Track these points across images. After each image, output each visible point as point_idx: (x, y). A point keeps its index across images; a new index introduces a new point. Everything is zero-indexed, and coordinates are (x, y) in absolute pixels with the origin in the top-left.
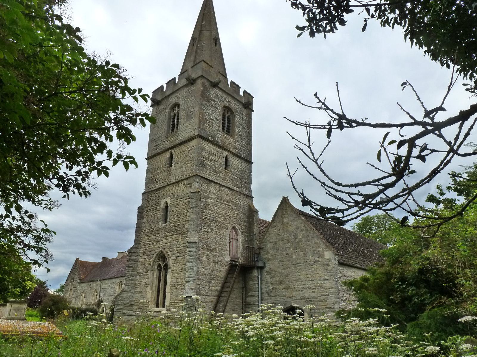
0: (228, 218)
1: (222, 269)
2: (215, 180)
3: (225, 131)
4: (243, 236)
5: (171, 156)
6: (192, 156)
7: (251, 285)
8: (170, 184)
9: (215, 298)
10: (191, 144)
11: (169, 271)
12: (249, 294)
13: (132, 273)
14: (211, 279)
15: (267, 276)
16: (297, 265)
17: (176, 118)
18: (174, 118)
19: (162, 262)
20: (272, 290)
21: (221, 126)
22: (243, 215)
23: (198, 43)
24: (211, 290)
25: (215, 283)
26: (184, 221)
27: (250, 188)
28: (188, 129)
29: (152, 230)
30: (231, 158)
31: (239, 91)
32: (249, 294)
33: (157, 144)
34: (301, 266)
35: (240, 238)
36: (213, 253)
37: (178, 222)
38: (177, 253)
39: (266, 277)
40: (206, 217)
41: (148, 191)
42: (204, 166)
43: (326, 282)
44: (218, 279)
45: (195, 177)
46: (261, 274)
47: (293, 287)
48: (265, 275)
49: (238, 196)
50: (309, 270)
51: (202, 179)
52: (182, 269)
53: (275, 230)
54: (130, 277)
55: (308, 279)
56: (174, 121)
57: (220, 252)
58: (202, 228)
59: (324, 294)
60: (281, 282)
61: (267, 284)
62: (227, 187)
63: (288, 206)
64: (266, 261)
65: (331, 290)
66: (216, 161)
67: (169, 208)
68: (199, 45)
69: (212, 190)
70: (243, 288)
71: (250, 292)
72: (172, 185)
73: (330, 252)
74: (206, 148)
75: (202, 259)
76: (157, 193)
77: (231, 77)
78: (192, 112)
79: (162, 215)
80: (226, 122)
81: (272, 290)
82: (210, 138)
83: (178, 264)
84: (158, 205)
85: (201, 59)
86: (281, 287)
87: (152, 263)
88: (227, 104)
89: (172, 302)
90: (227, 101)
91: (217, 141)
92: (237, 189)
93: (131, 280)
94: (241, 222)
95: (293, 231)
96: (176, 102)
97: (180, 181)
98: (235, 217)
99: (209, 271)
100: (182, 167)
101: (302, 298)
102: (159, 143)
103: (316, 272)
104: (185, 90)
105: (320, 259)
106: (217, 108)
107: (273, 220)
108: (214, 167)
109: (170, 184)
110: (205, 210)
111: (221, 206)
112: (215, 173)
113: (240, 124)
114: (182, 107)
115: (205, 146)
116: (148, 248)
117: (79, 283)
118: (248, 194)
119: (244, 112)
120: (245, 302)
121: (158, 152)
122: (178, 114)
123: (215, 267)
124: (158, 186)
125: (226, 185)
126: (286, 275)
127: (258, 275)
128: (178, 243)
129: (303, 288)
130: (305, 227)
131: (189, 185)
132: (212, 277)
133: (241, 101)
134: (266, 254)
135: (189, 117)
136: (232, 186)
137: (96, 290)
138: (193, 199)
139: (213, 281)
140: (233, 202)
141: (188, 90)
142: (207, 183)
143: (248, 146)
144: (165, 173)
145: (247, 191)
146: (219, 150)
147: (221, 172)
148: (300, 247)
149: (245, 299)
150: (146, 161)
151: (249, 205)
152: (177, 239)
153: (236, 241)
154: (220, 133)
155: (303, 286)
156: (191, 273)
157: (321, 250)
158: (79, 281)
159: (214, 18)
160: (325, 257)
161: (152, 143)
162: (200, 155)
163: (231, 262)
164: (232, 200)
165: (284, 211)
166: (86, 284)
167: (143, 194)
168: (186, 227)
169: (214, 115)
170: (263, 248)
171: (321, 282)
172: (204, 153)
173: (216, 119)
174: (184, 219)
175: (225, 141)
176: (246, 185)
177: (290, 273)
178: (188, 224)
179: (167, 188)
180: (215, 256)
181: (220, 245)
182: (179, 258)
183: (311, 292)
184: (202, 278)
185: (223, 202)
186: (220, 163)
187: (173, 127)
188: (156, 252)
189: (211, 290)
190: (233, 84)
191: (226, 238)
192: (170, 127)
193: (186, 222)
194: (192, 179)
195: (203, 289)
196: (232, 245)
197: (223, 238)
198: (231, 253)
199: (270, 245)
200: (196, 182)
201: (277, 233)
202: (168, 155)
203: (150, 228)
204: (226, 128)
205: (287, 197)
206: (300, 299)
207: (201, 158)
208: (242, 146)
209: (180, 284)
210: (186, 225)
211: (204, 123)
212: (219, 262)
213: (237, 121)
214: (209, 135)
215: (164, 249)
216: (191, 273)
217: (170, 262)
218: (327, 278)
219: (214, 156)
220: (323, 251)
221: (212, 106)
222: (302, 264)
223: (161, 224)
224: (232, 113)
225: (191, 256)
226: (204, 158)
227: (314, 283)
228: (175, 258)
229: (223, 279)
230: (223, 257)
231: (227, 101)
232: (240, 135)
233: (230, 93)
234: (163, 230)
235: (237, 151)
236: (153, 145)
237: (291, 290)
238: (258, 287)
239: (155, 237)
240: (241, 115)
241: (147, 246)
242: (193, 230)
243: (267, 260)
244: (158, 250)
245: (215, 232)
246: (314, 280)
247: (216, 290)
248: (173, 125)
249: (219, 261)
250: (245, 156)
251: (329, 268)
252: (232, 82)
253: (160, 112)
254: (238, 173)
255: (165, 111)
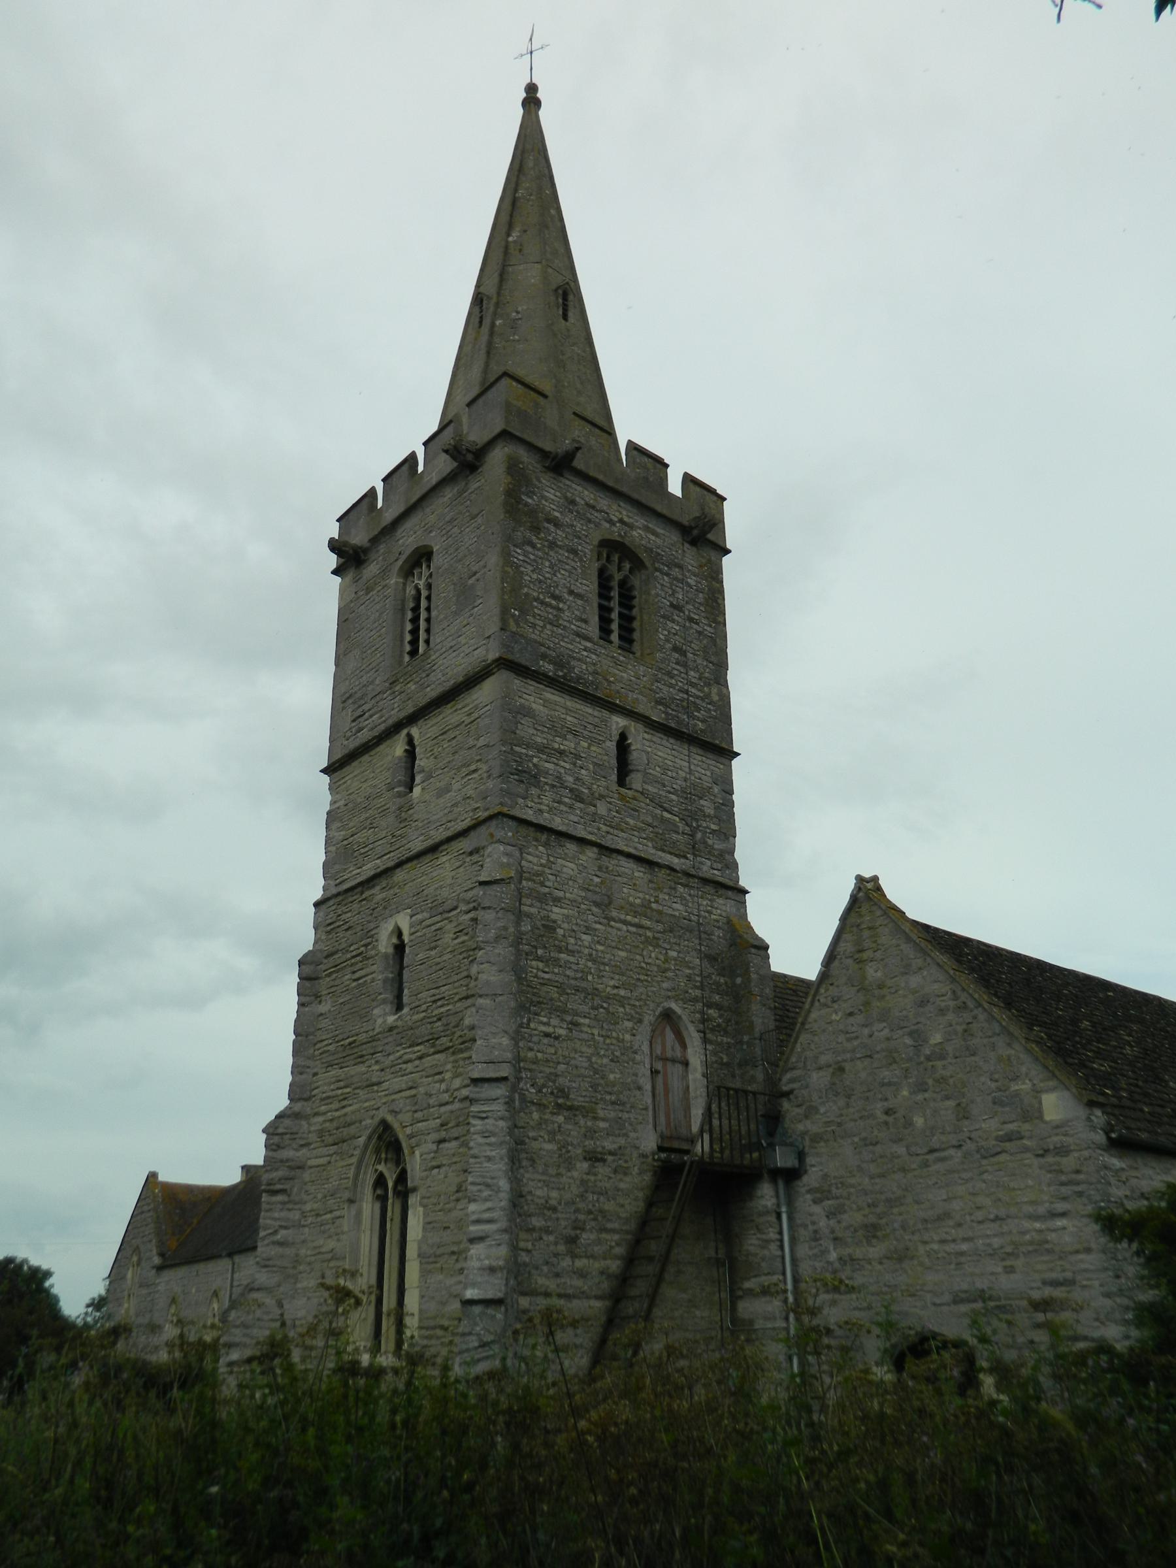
0: (642, 977)
1: (622, 1185)
2: (581, 832)
3: (615, 637)
4: (709, 1047)
5: (411, 754)
6: (482, 742)
7: (752, 1249)
8: (409, 860)
9: (598, 1304)
10: (474, 697)
11: (413, 1200)
12: (747, 1285)
13: (283, 1214)
14: (579, 1226)
15: (817, 1209)
16: (930, 1157)
17: (424, 604)
18: (416, 609)
19: (389, 1165)
20: (837, 1265)
21: (595, 620)
22: (706, 963)
23: (495, 315)
24: (582, 1274)
25: (599, 1242)
26: (461, 999)
27: (732, 852)
28: (464, 641)
29: (350, 1044)
30: (640, 739)
31: (664, 481)
32: (747, 1285)
33: (359, 712)
34: (951, 1158)
35: (696, 1056)
36: (582, 1122)
37: (439, 1003)
38: (442, 1125)
39: (811, 1210)
40: (547, 976)
41: (334, 891)
42: (527, 776)
43: (1059, 1223)
44: (609, 1226)
45: (494, 822)
46: (790, 1204)
47: (922, 1249)
48: (805, 1203)
49: (680, 889)
50: (985, 1176)
51: (523, 830)
52: (457, 1191)
53: (834, 1017)
54: (275, 1232)
55: (979, 1215)
56: (415, 620)
57: (613, 1115)
58: (529, 1020)
59: (1054, 1275)
60: (872, 1232)
61: (816, 1240)
62: (629, 856)
63: (879, 913)
64: (807, 1143)
65: (1082, 1261)
66: (578, 757)
67: (407, 950)
68: (498, 322)
69: (569, 868)
70: (719, 1263)
71: (748, 1279)
72: (415, 862)
73: (1066, 1094)
74: (534, 706)
75: (535, 1145)
76: (364, 896)
77: (626, 431)
78: (475, 573)
79: (385, 981)
80: (615, 604)
81: (837, 1265)
82: (548, 668)
83: (443, 1169)
84: (369, 944)
85: (501, 369)
86: (875, 1251)
87: (353, 1169)
88: (615, 533)
89: (427, 1328)
90: (611, 522)
91: (579, 678)
92: (675, 861)
93: (280, 1244)
94: (698, 993)
95: (904, 1013)
96: (421, 544)
97: (441, 843)
98: (670, 974)
99: (567, 1196)
100: (447, 789)
101: (963, 1295)
102: (366, 707)
103: (1012, 1185)
104: (449, 493)
105: (1027, 1126)
106: (574, 552)
107: (824, 976)
108: (571, 779)
109: (409, 860)
110: (540, 952)
111: (609, 929)
112: (579, 805)
113: (672, 605)
114: (437, 560)
115: (532, 699)
116: (337, 1114)
117: (160, 1268)
118: (721, 879)
119: (690, 557)
120: (734, 1321)
121: (364, 741)
122: (429, 587)
123: (592, 1178)
124: (368, 870)
125: (626, 849)
126: (888, 1200)
127: (778, 1205)
128: (443, 1086)
129: (962, 1254)
130: (955, 997)
131: (475, 858)
132: (581, 1217)
133: (675, 516)
134: (806, 1117)
135: (465, 596)
136: (653, 851)
137: (216, 1294)
138: (489, 908)
139: (586, 1237)
140: (660, 912)
141: (460, 493)
142: (546, 845)
143: (714, 690)
144: (391, 819)
145: (719, 866)
146: (590, 711)
147: (601, 797)
148: (941, 1081)
149: (734, 1309)
150: (326, 779)
151: (729, 922)
152: (436, 1070)
153: (679, 1068)
154: (589, 645)
155: (964, 1247)
156: (489, 1204)
157: (1024, 1086)
158: (157, 1260)
159: (553, 212)
160: (1047, 1118)
161: (343, 708)
162: (510, 737)
163: (663, 1155)
164: (654, 906)
165: (866, 933)
166: (182, 1272)
167: (317, 905)
168: (467, 1022)
169: (562, 578)
170: (791, 1092)
171: (1038, 1225)
172: (526, 729)
173: (571, 592)
174: (463, 991)
175: (614, 675)
176: (710, 842)
177: (906, 1190)
178: (473, 1010)
179: (400, 875)
180: (590, 1133)
181: (609, 1089)
182: (446, 1145)
183: (1000, 1269)
184: (537, 1222)
185: (614, 914)
186: (595, 764)
187: (414, 642)
188: (366, 1128)
189: (582, 1274)
190: (635, 453)
191: (638, 1057)
192: (402, 640)
193: (470, 1001)
194: (483, 830)
195: (545, 1269)
196: (665, 1084)
197: (625, 1058)
198: (662, 1119)
199: (819, 1079)
200: (499, 841)
201: (841, 1027)
202: (398, 748)
203: (345, 1036)
204: (615, 626)
205: (875, 879)
206: (956, 1301)
207: (517, 749)
208: (687, 692)
209: (453, 1253)
210: (468, 1012)
211: (524, 612)
212: (610, 1158)
213: (657, 595)
214: (544, 657)
215: (394, 1112)
216: (489, 1204)
217: (415, 1164)
218: (1061, 1207)
219: (569, 736)
220: (1037, 1092)
221: (553, 545)
222: (952, 1152)
223: (384, 1017)
224: (638, 564)
225: (486, 1134)
226: (528, 746)
227: (1005, 1229)
228: (434, 1147)
229: (633, 1226)
230: (626, 1135)
231: (611, 522)
232: (676, 649)
233: (625, 489)
234: (390, 1039)
235: (667, 713)
236: (348, 715)
237: (916, 1262)
238: (779, 1253)
239: (362, 1068)
240: (676, 572)
241: (333, 1106)
242: (494, 1029)
243: (812, 1140)
244: (372, 1117)
245: (585, 1036)
246: (1008, 1217)
247: (602, 1273)
248: (415, 632)
249: (611, 1153)
250: (702, 731)
251: (1069, 1162)
252: (633, 447)
253: (368, 590)
254: (673, 797)
255: (383, 583)
